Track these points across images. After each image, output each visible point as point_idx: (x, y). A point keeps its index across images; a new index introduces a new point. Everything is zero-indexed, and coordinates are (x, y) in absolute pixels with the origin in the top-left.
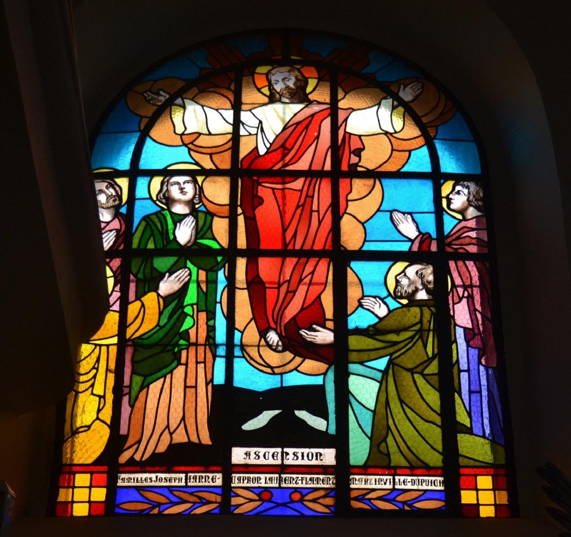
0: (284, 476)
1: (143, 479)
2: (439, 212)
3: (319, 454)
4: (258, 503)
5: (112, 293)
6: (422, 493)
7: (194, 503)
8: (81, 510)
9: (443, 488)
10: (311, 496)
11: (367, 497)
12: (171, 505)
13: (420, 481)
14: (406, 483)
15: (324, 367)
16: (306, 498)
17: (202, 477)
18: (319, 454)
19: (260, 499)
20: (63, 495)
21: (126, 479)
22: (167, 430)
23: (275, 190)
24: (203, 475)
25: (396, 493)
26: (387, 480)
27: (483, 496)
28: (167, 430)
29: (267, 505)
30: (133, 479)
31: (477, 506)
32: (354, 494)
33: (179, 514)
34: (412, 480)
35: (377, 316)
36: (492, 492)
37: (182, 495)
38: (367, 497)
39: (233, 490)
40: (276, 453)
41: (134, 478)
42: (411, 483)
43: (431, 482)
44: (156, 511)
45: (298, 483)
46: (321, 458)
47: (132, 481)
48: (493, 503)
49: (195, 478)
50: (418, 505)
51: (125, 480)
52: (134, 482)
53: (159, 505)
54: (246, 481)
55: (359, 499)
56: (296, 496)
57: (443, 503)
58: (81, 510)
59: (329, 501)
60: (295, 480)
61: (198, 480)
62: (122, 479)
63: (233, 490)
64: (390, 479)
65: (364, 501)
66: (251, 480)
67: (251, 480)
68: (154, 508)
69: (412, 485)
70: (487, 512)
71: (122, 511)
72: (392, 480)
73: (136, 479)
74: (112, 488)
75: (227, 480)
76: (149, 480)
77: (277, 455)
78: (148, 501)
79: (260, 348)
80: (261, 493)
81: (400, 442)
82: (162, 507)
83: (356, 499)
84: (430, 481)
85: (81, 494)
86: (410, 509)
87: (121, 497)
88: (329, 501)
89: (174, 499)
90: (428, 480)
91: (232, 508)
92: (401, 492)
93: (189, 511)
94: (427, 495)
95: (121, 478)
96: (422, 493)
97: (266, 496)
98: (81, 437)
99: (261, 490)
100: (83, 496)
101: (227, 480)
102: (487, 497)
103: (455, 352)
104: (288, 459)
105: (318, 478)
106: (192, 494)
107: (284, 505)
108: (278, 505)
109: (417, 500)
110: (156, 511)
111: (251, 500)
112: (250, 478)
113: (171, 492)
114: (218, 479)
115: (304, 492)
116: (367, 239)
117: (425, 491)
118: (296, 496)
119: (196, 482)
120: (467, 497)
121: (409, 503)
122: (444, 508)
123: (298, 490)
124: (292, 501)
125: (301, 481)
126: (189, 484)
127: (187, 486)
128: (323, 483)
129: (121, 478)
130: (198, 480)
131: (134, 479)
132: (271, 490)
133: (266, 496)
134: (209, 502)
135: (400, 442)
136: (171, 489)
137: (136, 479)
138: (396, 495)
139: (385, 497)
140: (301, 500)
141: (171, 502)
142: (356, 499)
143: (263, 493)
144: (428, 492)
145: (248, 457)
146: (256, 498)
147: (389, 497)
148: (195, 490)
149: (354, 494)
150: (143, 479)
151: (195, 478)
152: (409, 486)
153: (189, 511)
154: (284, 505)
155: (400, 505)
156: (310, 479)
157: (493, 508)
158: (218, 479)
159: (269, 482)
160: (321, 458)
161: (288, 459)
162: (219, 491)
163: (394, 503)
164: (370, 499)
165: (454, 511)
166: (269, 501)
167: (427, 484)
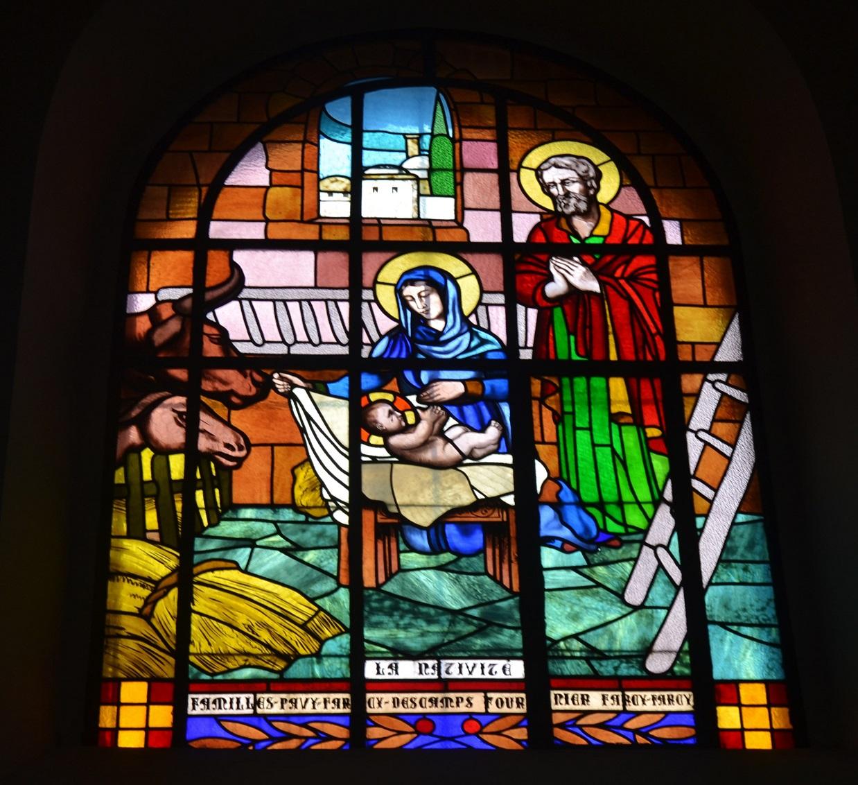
4: (407, 738)
5: (707, 587)
6: (662, 716)
7: (307, 738)
8: (130, 740)
11: (581, 722)
12: (318, 741)
14: (646, 702)
16: (485, 730)
17: (561, 696)
19: (419, 733)
21: (439, 700)
23: (717, 417)
24: (562, 693)
25: (624, 717)
26: (307, 701)
27: (752, 723)
33: (401, 748)
34: (394, 699)
35: (324, 178)
36: (765, 710)
37: (281, 726)
38: (581, 722)
39: (372, 718)
44: (251, 748)
47: (228, 705)
48: (768, 727)
51: (198, 705)
52: (231, 707)
54: (658, 702)
56: (473, 726)
57: (693, 732)
59: (521, 734)
62: (334, 702)
63: (372, 718)
64: (617, 696)
66: (630, 700)
70: (759, 741)
72: (620, 698)
74: (180, 715)
76: (410, 703)
78: (235, 737)
80: (417, 722)
81: (248, 579)
85: (132, 717)
87: (193, 730)
90: (512, 699)
92: (632, 715)
93: (649, 729)
94: (669, 719)
95: (331, 702)
96: (662, 716)
97: (423, 726)
98: (245, 649)
99: (418, 717)
100: (134, 718)
101: (358, 703)
103: (661, 409)
104: (496, 672)
105: (219, 699)
106: (305, 725)
107: (452, 739)
108: (442, 739)
109: (654, 726)
111: (400, 733)
113: (269, 723)
114: (386, 703)
115: (484, 720)
117: (667, 713)
118: (473, 726)
119: (338, 707)
120: (728, 717)
121: (643, 730)
122: (691, 741)
123: (474, 716)
124: (467, 734)
126: (490, 710)
127: (255, 714)
129: (331, 702)
131: (231, 703)
133: (423, 726)
135: (248, 579)
136: (269, 718)
138: (625, 719)
139: (611, 723)
142: (563, 726)
143: (421, 723)
144: (671, 716)
146: (411, 729)
147: (617, 722)
149: (558, 719)
152: (649, 706)
153: (649, 729)
154: (452, 739)
155: (630, 735)
156: (203, 702)
157: (767, 735)
158: (386, 703)
163: (621, 732)
164: (580, 727)
166: (431, 734)
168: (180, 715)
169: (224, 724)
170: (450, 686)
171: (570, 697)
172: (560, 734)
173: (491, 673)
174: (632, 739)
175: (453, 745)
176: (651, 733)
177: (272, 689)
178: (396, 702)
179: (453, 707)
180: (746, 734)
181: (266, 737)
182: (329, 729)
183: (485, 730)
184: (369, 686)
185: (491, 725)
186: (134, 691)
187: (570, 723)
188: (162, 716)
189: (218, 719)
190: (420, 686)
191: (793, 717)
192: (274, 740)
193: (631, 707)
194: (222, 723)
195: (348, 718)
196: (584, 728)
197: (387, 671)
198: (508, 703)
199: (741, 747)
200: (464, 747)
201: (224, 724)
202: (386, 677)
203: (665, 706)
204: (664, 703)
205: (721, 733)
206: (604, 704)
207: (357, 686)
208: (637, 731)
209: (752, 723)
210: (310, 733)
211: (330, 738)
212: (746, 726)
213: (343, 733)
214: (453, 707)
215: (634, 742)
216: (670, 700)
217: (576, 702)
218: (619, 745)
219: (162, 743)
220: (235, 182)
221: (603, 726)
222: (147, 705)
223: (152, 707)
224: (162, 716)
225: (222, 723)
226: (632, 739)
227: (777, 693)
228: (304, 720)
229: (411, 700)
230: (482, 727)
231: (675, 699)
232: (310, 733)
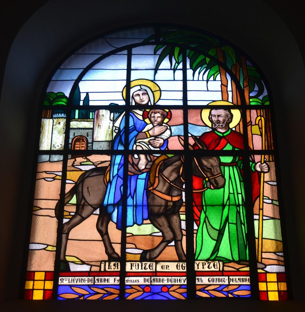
0: (231, 277)
1: (135, 281)
2: (185, 80)
3: (167, 266)
7: (104, 294)
8: (38, 296)
9: (249, 283)
10: (172, 289)
12: (108, 295)
13: (217, 279)
15: (58, 183)
16: (170, 290)
18: (167, 266)
19: (144, 291)
20: (30, 285)
22: (46, 249)
28: (46, 249)
29: (145, 295)
30: (129, 280)
31: (279, 291)
32: (198, 287)
34: (167, 279)
40: (163, 266)
41: (130, 280)
42: (166, 281)
43: (177, 280)
44: (82, 298)
45: (225, 282)
46: (168, 268)
47: (129, 282)
49: (98, 280)
50: (236, 293)
53: (83, 295)
55: (202, 290)
56: (165, 289)
58: (38, 296)
60: (223, 280)
61: (100, 281)
65: (204, 291)
66: (161, 280)
67: (161, 280)
68: (80, 297)
69: (167, 282)
71: (61, 299)
73: (131, 280)
74: (56, 285)
75: (122, 281)
76: (137, 281)
77: (164, 267)
78: (77, 293)
79: (144, 207)
82: (86, 297)
83: (200, 290)
84: (178, 280)
85: (39, 285)
86: (232, 296)
87: (61, 290)
88: (184, 290)
89: (92, 292)
91: (126, 295)
93: (232, 291)
94: (240, 288)
95: (117, 280)
96: (237, 286)
101: (122, 281)
102: (273, 286)
104: (211, 268)
105: (62, 279)
106: (102, 289)
110: (82, 298)
111: (139, 291)
112: (243, 279)
113: (90, 288)
115: (169, 287)
116: (121, 93)
117: (240, 285)
119: (99, 282)
120: (262, 286)
124: (162, 292)
125: (165, 281)
128: (84, 282)
129: (117, 280)
130: (100, 281)
132: (167, 286)
134: (98, 293)
136: (71, 286)
137: (131, 280)
139: (217, 289)
140: (168, 291)
141: (90, 294)
145: (116, 267)
146: (141, 290)
147: (220, 289)
148: (104, 287)
149: (198, 287)
150: (135, 281)
151: (98, 280)
153: (232, 291)
154: (158, 293)
159: (238, 281)
160: (168, 268)
161: (169, 269)
162: (118, 287)
164: (208, 291)
165: (257, 295)
167: (213, 281)
168: (56, 285)
169: (73, 288)
170: (158, 274)
171: (178, 280)
172: (199, 293)
173: (145, 268)
174: (227, 295)
175: (159, 297)
176: (233, 293)
177: (90, 275)
178: (145, 280)
179: (247, 282)
180: (269, 293)
181: (88, 293)
182: (112, 290)
183: (170, 290)
184: (197, 274)
185: (109, 288)
186: (40, 276)
187: (202, 289)
188: (49, 285)
189: (71, 286)
190: (136, 274)
191: (24, 285)
192: (91, 295)
193: (231, 283)
194: (72, 288)
195: (186, 286)
196: (209, 291)
197: (113, 267)
198: (213, 280)
199: (267, 300)
200: (175, 299)
201: (73, 288)
202: (112, 270)
203: (136, 283)
204: (240, 282)
205: (260, 292)
206: (114, 282)
207: (123, 274)
208: (228, 292)
209: (272, 290)
210: (106, 292)
211: (112, 294)
212: (42, 288)
213: (118, 292)
214: (247, 282)
215: (228, 296)
216: (221, 280)
217: (233, 281)
218: (206, 298)
219: (263, 298)
220: (87, 79)
221: (214, 290)
222: (45, 280)
223: (268, 281)
224: (49, 285)
225: (72, 288)
226: (227, 295)
227: (31, 276)
228: (103, 287)
229: (138, 280)
230: (169, 289)
231: (106, 280)
232: (106, 292)
